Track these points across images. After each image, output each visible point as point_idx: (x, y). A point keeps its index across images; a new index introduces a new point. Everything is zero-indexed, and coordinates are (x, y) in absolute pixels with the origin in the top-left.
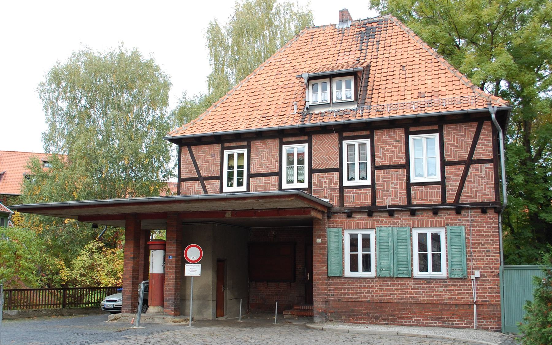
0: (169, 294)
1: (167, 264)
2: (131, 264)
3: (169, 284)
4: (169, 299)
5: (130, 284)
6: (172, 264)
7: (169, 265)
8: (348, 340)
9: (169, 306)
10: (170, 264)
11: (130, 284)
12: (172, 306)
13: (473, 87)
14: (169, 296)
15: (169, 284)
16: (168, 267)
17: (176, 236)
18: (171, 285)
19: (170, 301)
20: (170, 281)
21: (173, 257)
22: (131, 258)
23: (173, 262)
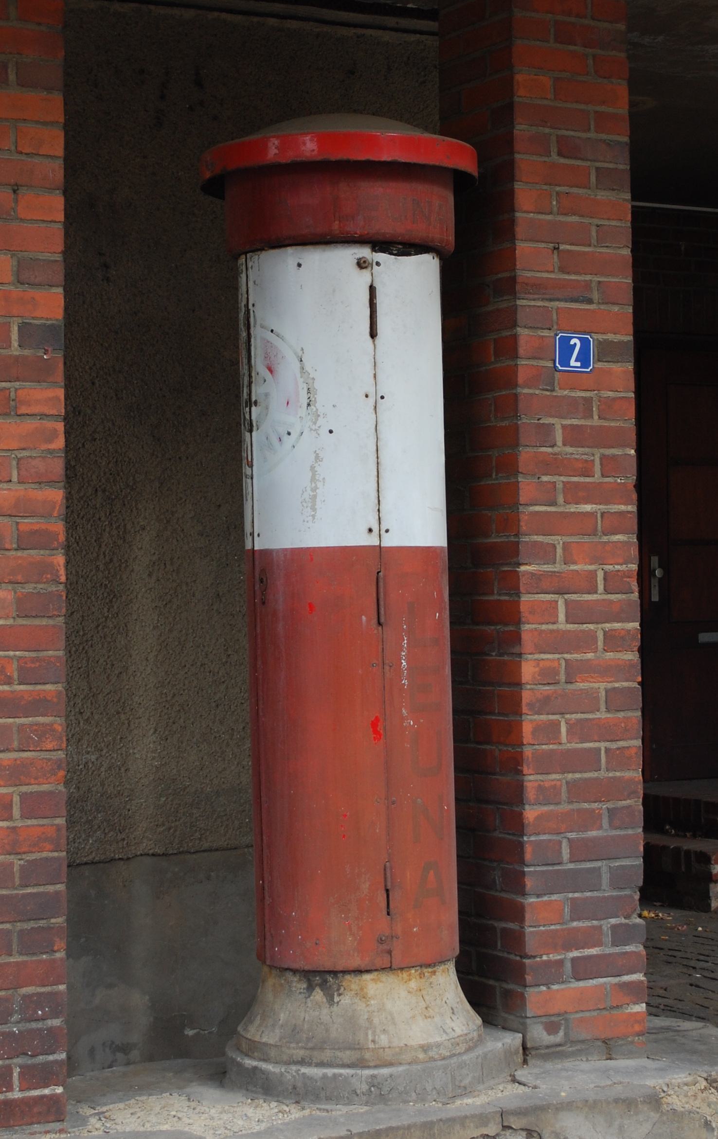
0: (577, 791)
1: (545, 433)
2: (243, 439)
3: (573, 672)
4: (581, 851)
5: (37, 706)
6: (601, 438)
7: (561, 448)
8: (121, 481)
9: (591, 938)
10: (574, 436)
11: (37, 706)
12: (621, 935)
13: (43, 485)
14: (590, 820)
15: (573, 672)
16: (554, 465)
17: (623, 110)
18: (601, 686)
19: (589, 881)
20: (586, 642)
21: (606, 351)
22: (304, 989)
23: (607, 407)
